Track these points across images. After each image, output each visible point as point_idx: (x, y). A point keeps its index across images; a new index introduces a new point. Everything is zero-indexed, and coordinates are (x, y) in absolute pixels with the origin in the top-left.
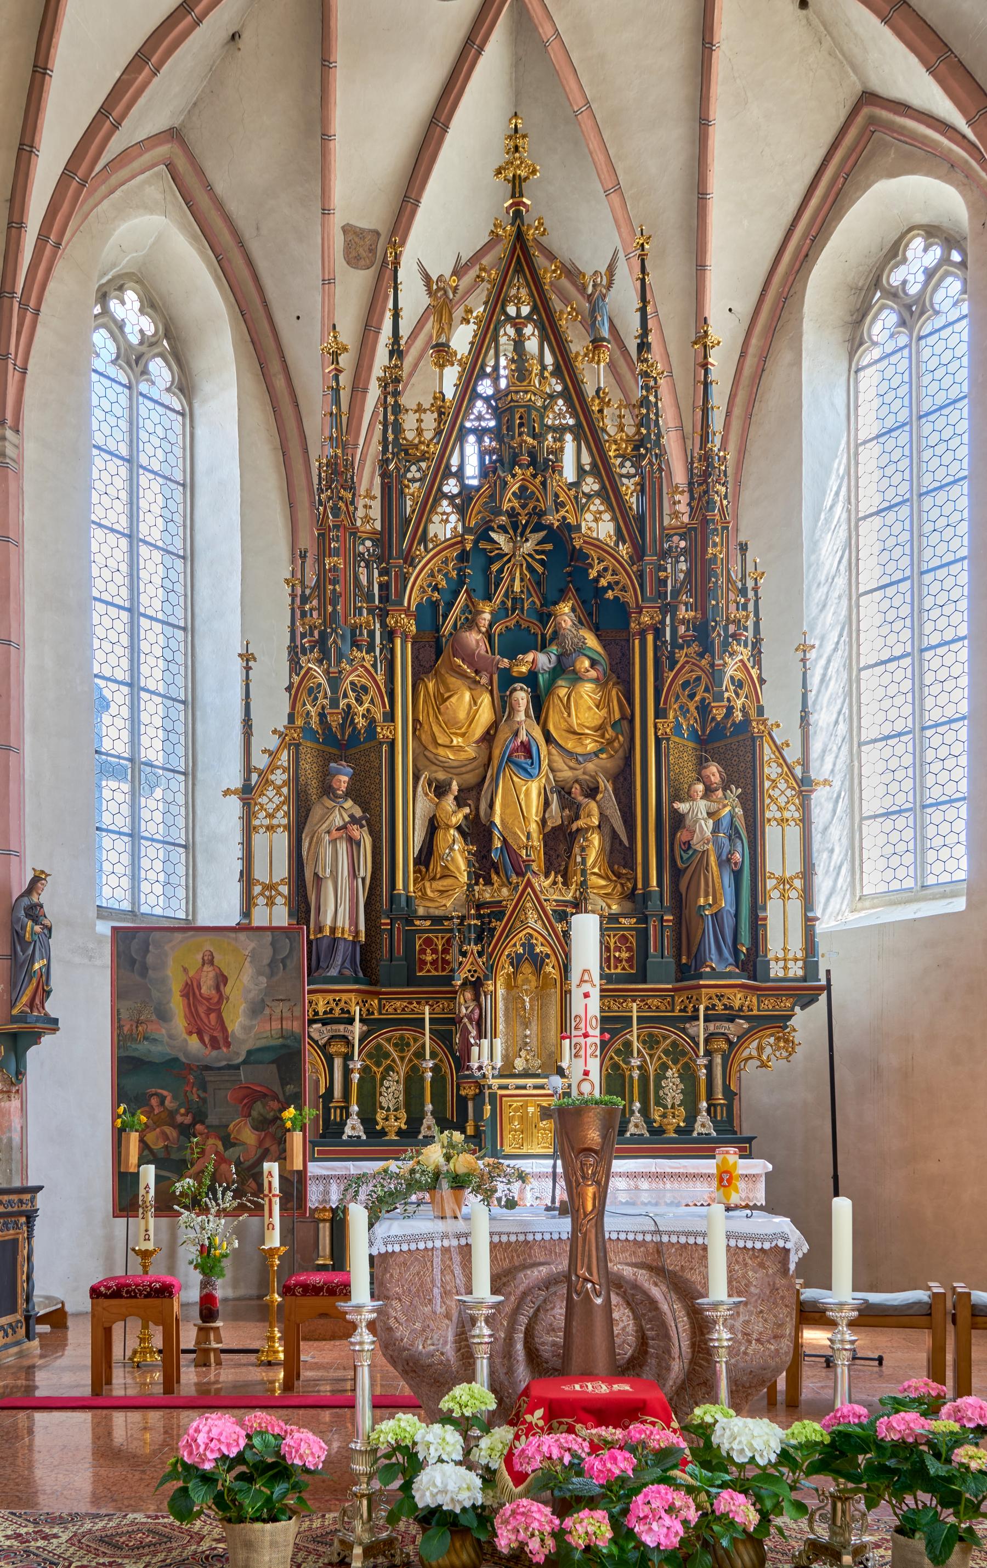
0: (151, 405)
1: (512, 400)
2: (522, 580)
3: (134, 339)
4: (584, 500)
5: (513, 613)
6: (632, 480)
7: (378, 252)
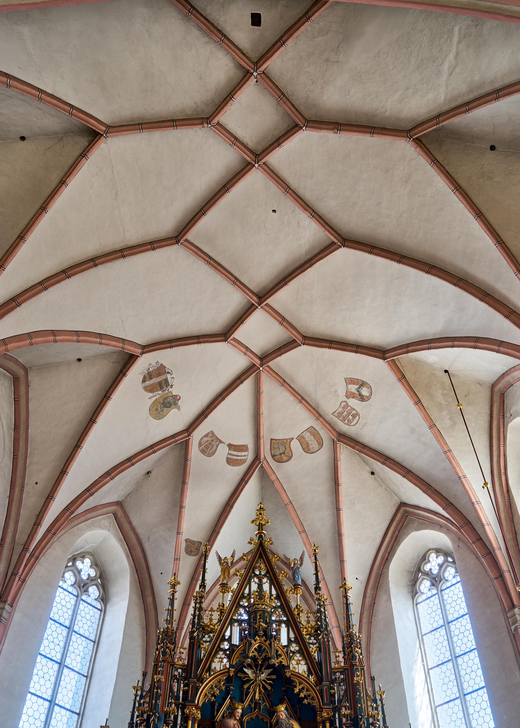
0: (86, 605)
1: (256, 608)
2: (260, 693)
4: (291, 655)
5: (254, 711)
6: (315, 646)
7: (200, 551)
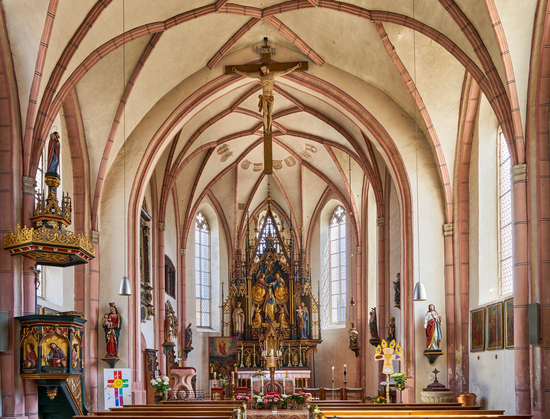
3: (200, 222)
7: (245, 207)
